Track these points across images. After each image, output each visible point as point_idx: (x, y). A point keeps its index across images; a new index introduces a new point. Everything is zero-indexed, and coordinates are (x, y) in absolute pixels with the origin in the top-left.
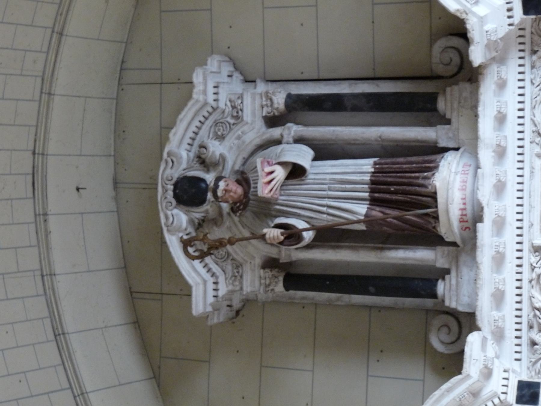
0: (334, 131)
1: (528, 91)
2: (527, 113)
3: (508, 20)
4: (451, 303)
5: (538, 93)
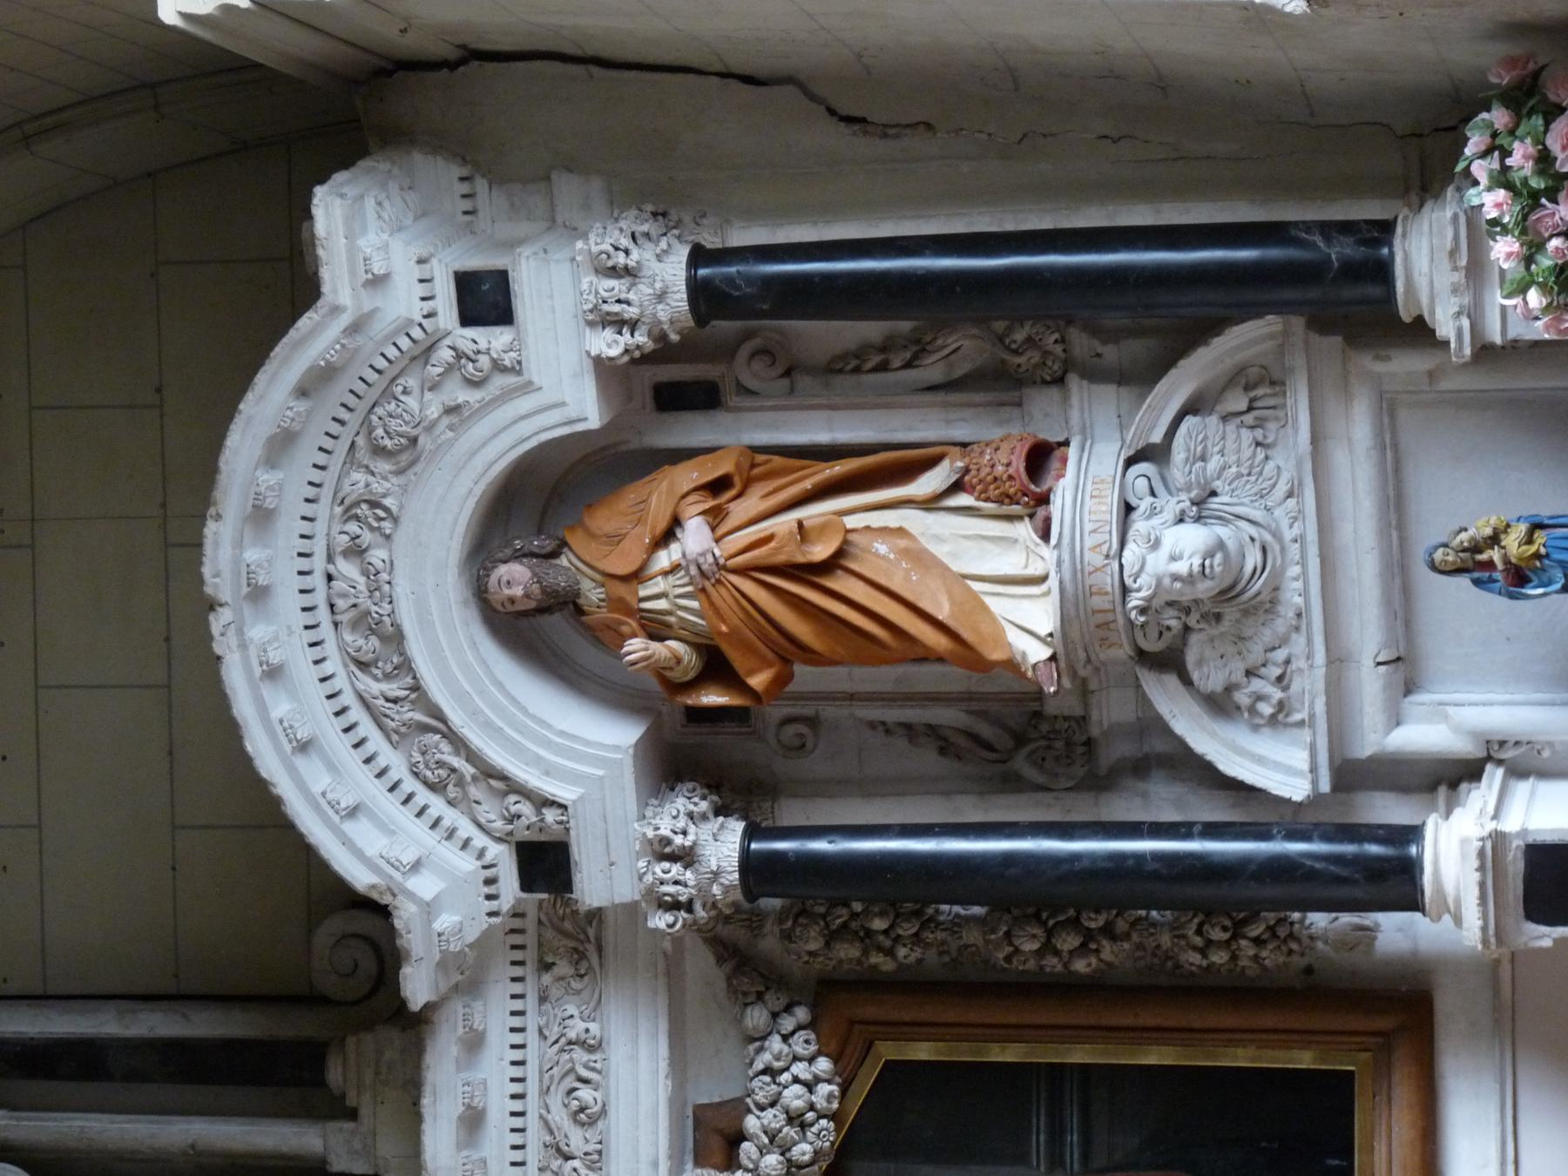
0: (82, 1128)
1: (532, 1054)
2: (532, 1104)
3: (486, 902)
5: (556, 1058)
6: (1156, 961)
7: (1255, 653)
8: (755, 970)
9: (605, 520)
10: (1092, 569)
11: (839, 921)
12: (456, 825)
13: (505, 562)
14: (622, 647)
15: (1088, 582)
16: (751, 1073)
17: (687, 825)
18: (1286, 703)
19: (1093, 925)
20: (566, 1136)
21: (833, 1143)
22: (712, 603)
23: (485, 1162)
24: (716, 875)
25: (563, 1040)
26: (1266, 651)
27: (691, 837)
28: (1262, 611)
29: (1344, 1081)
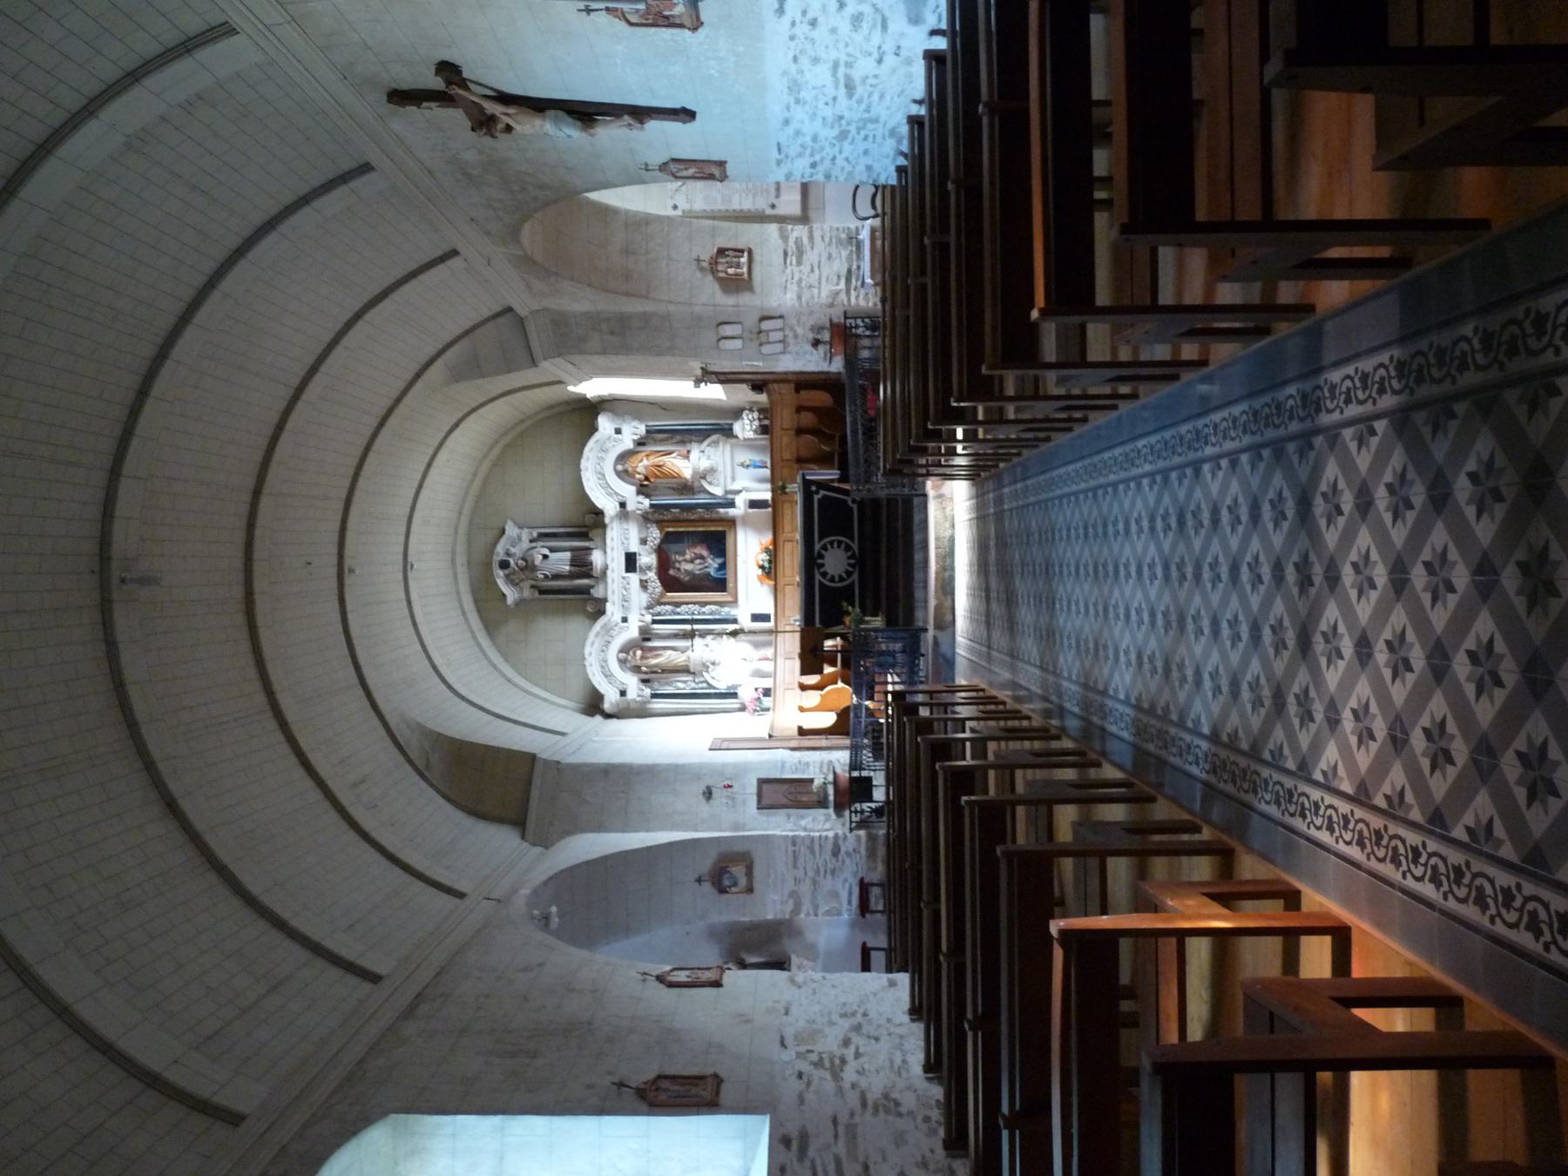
4: (596, 596)
9: (631, 460)
17: (611, 522)
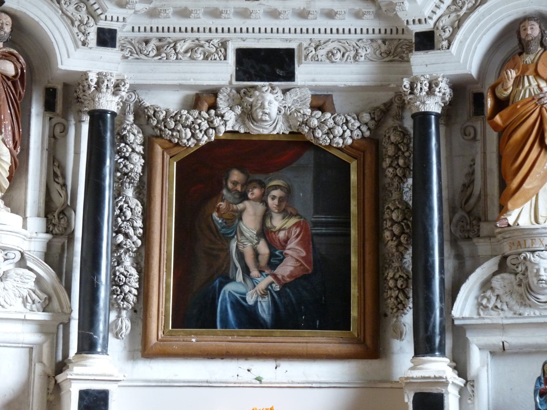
1: (353, 36)
2: (335, 36)
5: (351, 45)
6: (388, 261)
7: (506, 299)
8: (382, 117)
10: (542, 240)
11: (402, 147)
12: (441, 9)
13: (540, 27)
14: (513, 69)
15: (537, 239)
16: (346, 115)
18: (486, 309)
19: (402, 238)
20: (323, 48)
21: (321, 144)
22: (528, 102)
23: (315, 19)
24: (424, 103)
25: (358, 48)
26: (506, 302)
27: (438, 94)
28: (522, 301)
29: (346, 326)
